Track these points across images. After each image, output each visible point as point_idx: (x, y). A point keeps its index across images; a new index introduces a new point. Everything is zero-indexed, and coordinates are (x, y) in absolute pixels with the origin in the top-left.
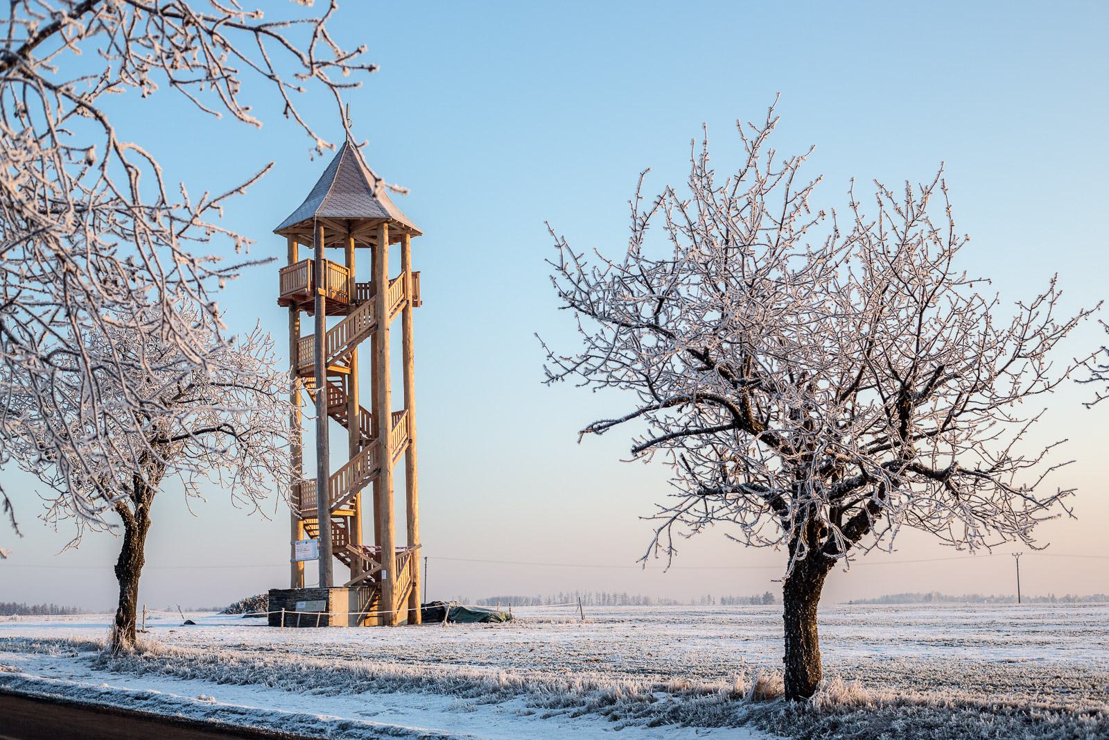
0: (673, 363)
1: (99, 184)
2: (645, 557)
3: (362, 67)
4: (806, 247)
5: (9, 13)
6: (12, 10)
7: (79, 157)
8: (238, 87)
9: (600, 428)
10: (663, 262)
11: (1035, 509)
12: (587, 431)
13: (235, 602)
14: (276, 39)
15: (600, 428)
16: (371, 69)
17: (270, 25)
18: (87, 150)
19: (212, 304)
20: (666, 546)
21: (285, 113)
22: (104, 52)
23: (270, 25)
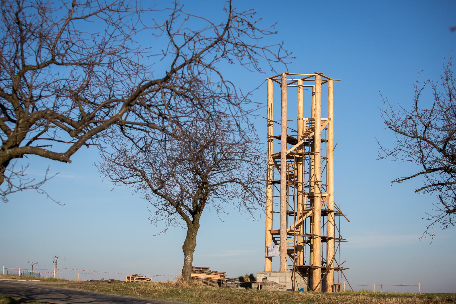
0: (39, 75)
1: (189, 72)
2: (421, 238)
3: (293, 58)
4: (252, 123)
5: (247, 95)
6: (253, 102)
7: (216, 85)
8: (258, 64)
9: (400, 180)
10: (427, 111)
11: (16, 44)
12: (394, 182)
13: (243, 275)
14: (268, 51)
15: (400, 180)
16: (295, 58)
17: (266, 47)
18: (218, 83)
19: (253, 124)
20: (431, 234)
21: (272, 70)
22: (251, 95)
23: (266, 47)
